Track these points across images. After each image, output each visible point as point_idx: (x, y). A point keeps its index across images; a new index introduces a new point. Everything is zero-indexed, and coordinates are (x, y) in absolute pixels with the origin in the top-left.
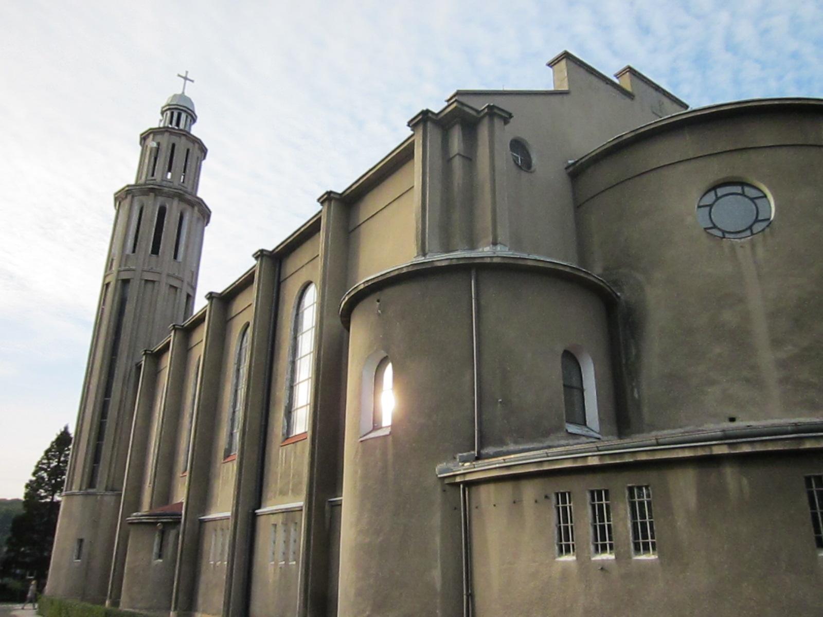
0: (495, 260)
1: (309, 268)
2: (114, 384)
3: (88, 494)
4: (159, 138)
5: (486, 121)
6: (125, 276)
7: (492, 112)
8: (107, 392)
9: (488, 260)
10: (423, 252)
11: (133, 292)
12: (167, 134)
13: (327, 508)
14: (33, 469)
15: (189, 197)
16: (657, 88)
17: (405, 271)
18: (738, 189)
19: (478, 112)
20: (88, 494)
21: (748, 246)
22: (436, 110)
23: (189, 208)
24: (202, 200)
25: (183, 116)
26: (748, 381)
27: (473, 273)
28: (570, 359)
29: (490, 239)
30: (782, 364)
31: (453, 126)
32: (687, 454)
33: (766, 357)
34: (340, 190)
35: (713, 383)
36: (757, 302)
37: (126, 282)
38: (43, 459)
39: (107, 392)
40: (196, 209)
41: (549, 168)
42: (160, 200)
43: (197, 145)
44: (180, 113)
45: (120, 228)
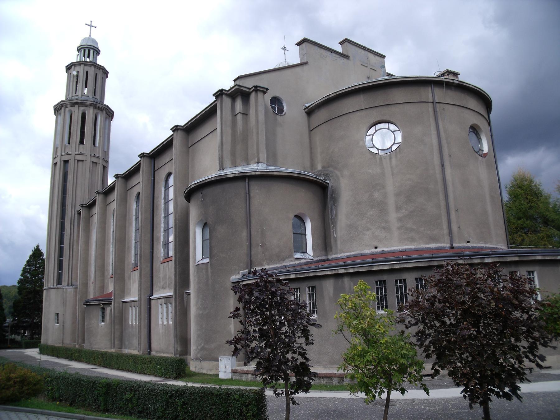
0: (257, 173)
1: (171, 164)
2: (66, 224)
3: (58, 288)
4: (77, 68)
5: (253, 94)
6: (66, 158)
7: (256, 89)
8: (62, 228)
9: (253, 174)
10: (222, 168)
11: (71, 167)
12: (82, 66)
13: (185, 296)
14: (21, 272)
15: (100, 105)
16: (365, 48)
17: (213, 179)
18: (386, 125)
19: (250, 89)
20: (58, 288)
21: (388, 158)
22: (227, 88)
23: (100, 112)
24: (107, 106)
25: (92, 52)
26: (384, 228)
27: (247, 180)
28: (300, 219)
29: (256, 160)
30: (400, 220)
31: (237, 96)
32: (329, 273)
33: (393, 216)
34: (182, 124)
35: (369, 229)
36: (390, 188)
37: (66, 162)
38: (26, 266)
39: (62, 228)
40: (104, 112)
41: (293, 111)
42: (82, 108)
43: (101, 70)
44: (89, 50)
45: (59, 128)
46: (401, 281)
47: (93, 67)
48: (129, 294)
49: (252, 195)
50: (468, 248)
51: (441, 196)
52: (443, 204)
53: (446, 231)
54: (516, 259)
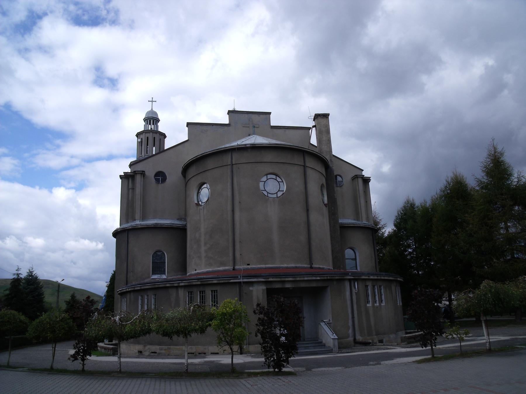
12: (144, 134)
33: (203, 249)
36: (203, 230)
46: (191, 292)
47: (151, 133)
48: (263, 290)
49: (129, 241)
50: (248, 269)
51: (230, 233)
52: (231, 239)
53: (231, 258)
54: (199, 283)
